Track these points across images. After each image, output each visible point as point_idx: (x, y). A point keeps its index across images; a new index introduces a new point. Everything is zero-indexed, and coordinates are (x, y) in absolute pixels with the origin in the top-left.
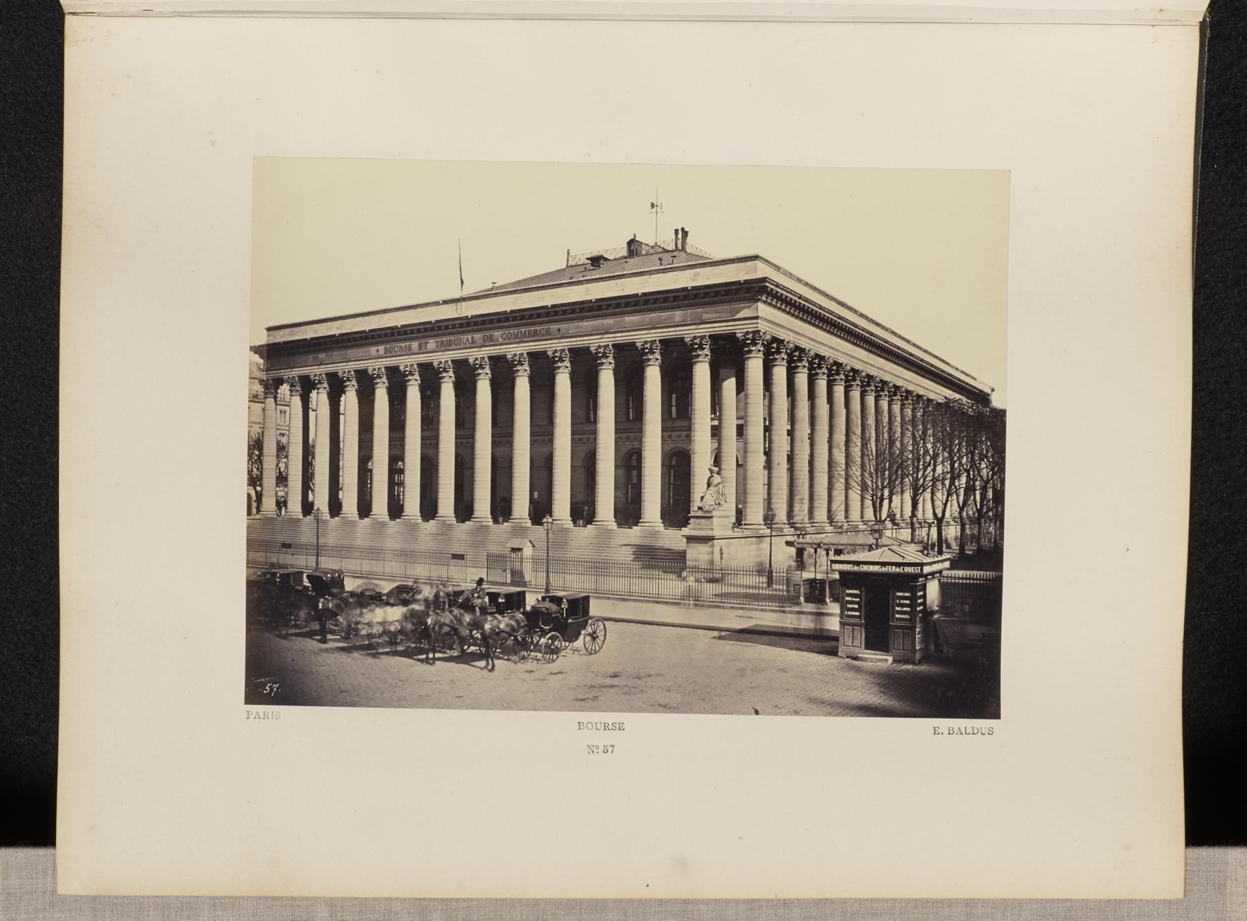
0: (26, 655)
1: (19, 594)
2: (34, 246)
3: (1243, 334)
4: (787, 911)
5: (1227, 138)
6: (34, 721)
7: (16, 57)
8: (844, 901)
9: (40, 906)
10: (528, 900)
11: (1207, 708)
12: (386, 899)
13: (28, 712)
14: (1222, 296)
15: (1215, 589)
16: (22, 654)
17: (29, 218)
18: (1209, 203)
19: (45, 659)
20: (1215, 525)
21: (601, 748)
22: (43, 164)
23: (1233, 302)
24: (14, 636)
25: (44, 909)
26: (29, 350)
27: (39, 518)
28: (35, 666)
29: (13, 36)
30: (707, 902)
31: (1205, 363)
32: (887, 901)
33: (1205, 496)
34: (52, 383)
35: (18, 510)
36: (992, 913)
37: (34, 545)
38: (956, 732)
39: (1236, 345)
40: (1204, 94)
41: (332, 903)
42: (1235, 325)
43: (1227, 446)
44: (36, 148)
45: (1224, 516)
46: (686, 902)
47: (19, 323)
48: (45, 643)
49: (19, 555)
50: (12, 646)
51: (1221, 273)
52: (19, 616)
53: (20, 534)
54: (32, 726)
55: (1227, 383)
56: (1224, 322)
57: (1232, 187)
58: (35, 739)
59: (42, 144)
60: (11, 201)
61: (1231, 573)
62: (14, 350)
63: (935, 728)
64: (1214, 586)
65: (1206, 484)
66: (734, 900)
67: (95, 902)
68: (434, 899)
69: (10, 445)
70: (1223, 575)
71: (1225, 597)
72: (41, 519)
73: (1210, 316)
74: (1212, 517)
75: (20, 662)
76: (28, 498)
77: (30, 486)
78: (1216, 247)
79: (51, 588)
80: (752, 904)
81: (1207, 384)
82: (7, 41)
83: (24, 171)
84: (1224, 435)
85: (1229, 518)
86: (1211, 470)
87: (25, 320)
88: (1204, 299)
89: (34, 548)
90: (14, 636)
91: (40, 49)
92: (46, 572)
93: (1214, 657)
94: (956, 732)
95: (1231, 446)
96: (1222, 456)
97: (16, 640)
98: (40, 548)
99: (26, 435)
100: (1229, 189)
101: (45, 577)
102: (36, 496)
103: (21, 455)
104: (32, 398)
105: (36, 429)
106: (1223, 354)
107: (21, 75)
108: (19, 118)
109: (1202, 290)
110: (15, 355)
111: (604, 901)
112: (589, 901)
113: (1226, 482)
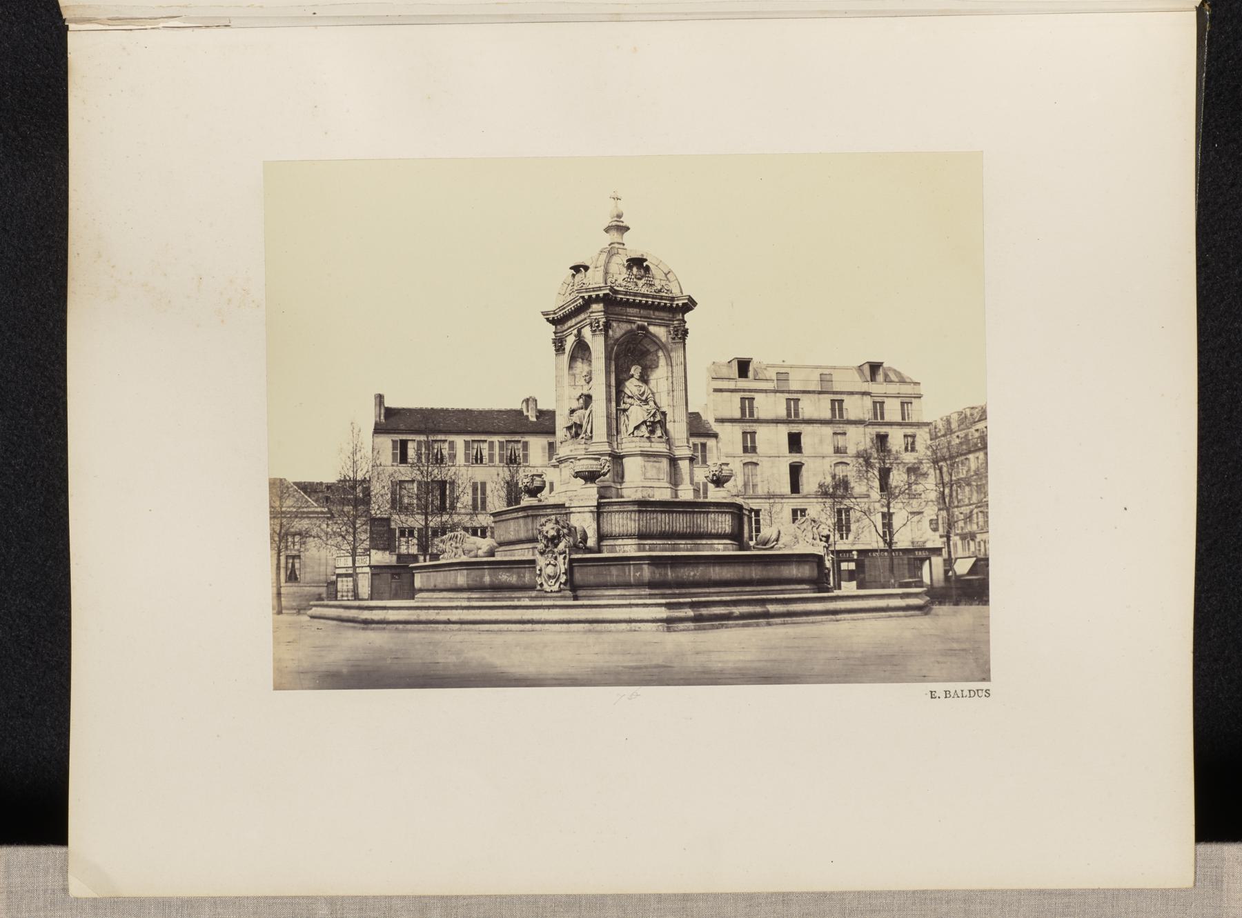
1: (13, 576)
2: (28, 225)
5: (1228, 117)
6: (29, 704)
7: (15, 40)
9: (41, 904)
10: (527, 896)
11: (1207, 691)
12: (386, 897)
13: (23, 694)
14: (1222, 276)
16: (18, 636)
17: (24, 197)
18: (1209, 182)
19: (40, 641)
22: (38, 143)
23: (1234, 282)
24: (9, 618)
25: (46, 907)
26: (23, 330)
27: (34, 499)
28: (30, 649)
29: (13, 18)
31: (1206, 343)
33: (1206, 478)
34: (47, 363)
36: (990, 910)
37: (29, 526)
38: (952, 696)
40: (1203, 88)
41: (332, 901)
42: (1235, 306)
43: (1228, 427)
44: (32, 128)
45: (1225, 498)
47: (14, 303)
48: (40, 625)
49: (14, 536)
50: (7, 629)
51: (1222, 253)
53: (15, 515)
54: (27, 709)
55: (1228, 364)
56: (1225, 302)
57: (1233, 166)
58: (30, 722)
59: (38, 124)
60: (6, 180)
63: (931, 692)
65: (1206, 465)
67: (95, 903)
68: (434, 897)
69: (5, 427)
70: (1223, 556)
71: (1226, 579)
72: (36, 500)
73: (1211, 296)
76: (23, 480)
77: (25, 467)
79: (46, 569)
81: (1208, 364)
82: (7, 24)
83: (20, 151)
85: (1229, 499)
86: (1212, 451)
88: (1205, 280)
89: (29, 529)
91: (39, 31)
93: (1215, 639)
94: (952, 696)
95: (1231, 427)
96: (1223, 437)
99: (21, 416)
100: (1230, 169)
101: (40, 558)
106: (1224, 334)
107: (20, 58)
108: (17, 100)
109: (1203, 269)
110: (10, 335)
111: (604, 897)
113: (1227, 463)
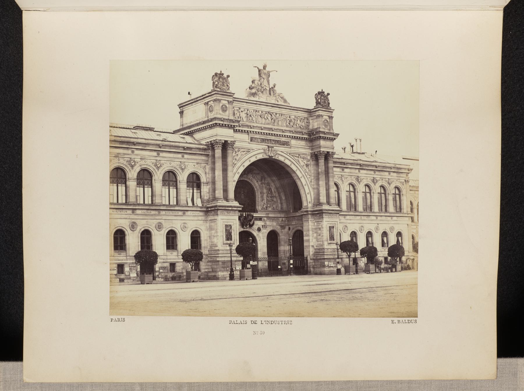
0: (7, 240)
1: (4, 214)
3: (521, 103)
4: (333, 386)
6: (10, 269)
8: (357, 382)
9: (19, 386)
15: (509, 212)
16: (6, 240)
19: (15, 242)
20: (509, 185)
21: (259, 332)
23: (517, 90)
24: (2, 232)
28: (11, 245)
30: (299, 382)
32: (375, 381)
35: (4, 179)
39: (518, 108)
41: (141, 384)
46: (290, 383)
47: (4, 99)
49: (4, 198)
51: (512, 77)
52: (4, 224)
55: (514, 124)
57: (517, 41)
61: (516, 206)
62: (2, 110)
64: (509, 211)
66: (310, 381)
73: (507, 95)
74: (508, 182)
75: (5, 243)
76: (8, 174)
77: (9, 168)
78: (510, 66)
79: (18, 212)
80: (318, 383)
84: (513, 147)
87: (7, 97)
90: (2, 232)
92: (15, 205)
95: (516, 151)
97: (3, 234)
98: (13, 195)
99: (7, 147)
101: (15, 207)
102: (11, 172)
103: (5, 155)
104: (10, 131)
105: (12, 144)
109: (504, 84)
110: (3, 113)
112: (250, 383)
113: (514, 167)
